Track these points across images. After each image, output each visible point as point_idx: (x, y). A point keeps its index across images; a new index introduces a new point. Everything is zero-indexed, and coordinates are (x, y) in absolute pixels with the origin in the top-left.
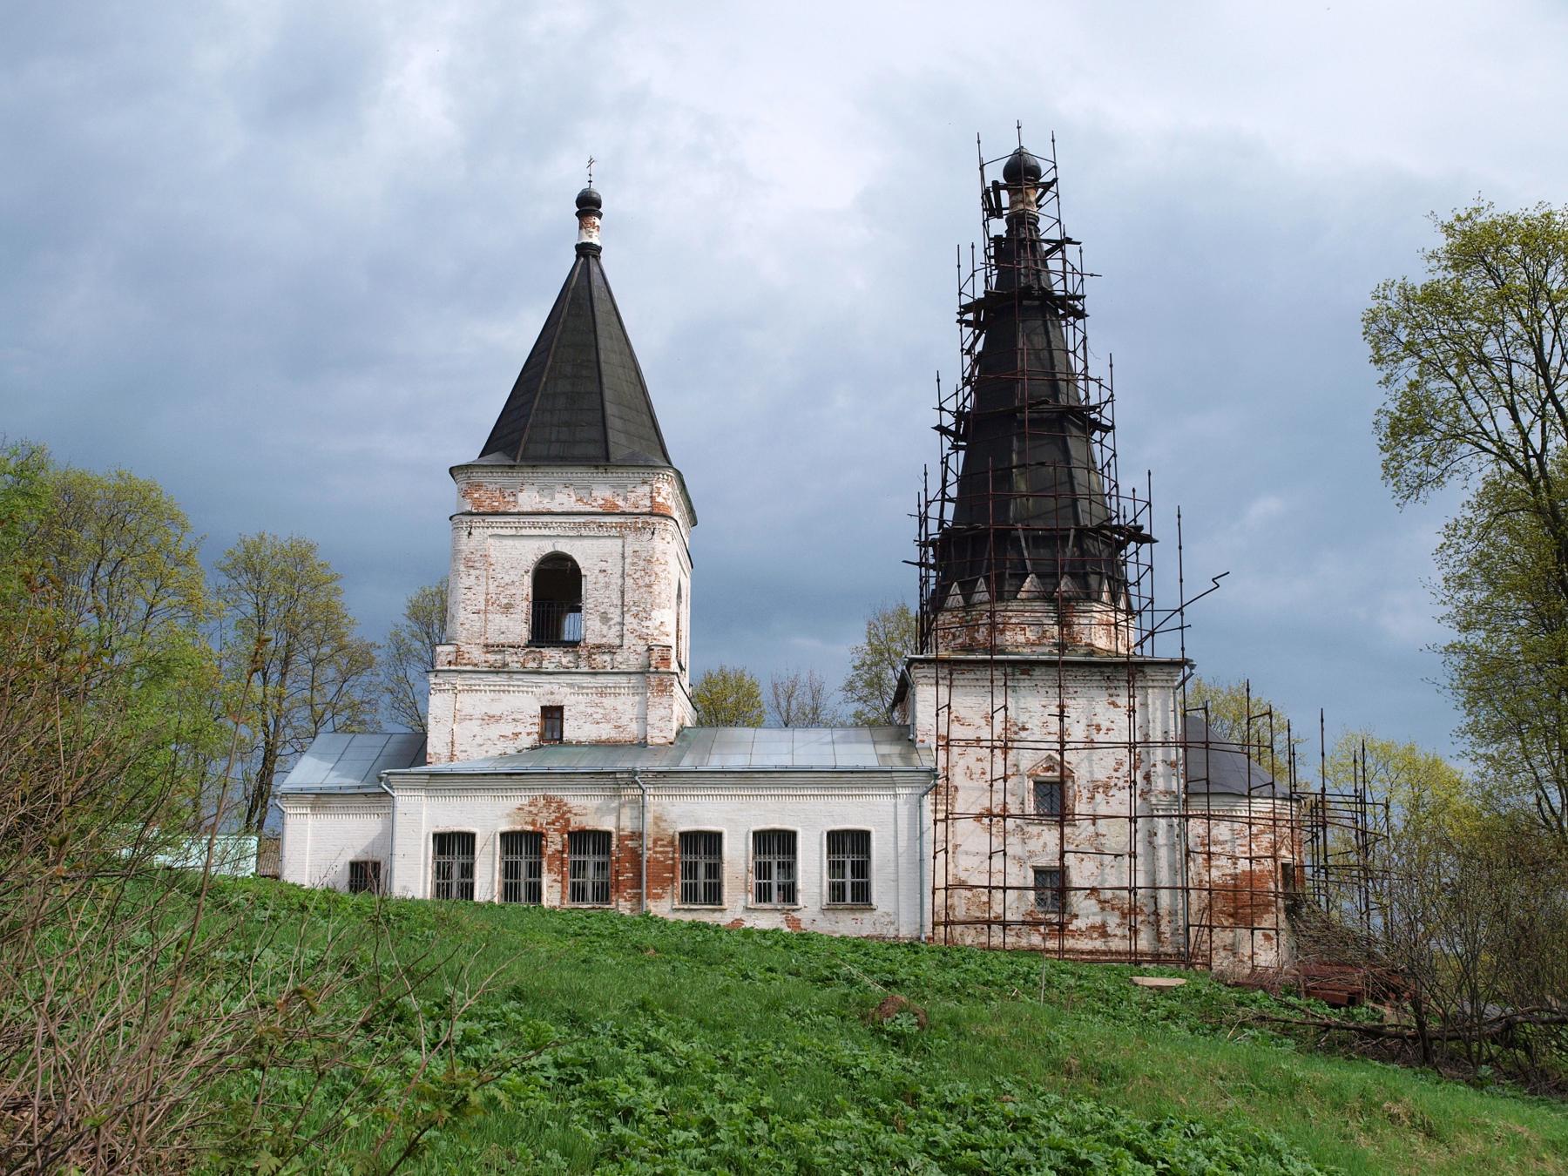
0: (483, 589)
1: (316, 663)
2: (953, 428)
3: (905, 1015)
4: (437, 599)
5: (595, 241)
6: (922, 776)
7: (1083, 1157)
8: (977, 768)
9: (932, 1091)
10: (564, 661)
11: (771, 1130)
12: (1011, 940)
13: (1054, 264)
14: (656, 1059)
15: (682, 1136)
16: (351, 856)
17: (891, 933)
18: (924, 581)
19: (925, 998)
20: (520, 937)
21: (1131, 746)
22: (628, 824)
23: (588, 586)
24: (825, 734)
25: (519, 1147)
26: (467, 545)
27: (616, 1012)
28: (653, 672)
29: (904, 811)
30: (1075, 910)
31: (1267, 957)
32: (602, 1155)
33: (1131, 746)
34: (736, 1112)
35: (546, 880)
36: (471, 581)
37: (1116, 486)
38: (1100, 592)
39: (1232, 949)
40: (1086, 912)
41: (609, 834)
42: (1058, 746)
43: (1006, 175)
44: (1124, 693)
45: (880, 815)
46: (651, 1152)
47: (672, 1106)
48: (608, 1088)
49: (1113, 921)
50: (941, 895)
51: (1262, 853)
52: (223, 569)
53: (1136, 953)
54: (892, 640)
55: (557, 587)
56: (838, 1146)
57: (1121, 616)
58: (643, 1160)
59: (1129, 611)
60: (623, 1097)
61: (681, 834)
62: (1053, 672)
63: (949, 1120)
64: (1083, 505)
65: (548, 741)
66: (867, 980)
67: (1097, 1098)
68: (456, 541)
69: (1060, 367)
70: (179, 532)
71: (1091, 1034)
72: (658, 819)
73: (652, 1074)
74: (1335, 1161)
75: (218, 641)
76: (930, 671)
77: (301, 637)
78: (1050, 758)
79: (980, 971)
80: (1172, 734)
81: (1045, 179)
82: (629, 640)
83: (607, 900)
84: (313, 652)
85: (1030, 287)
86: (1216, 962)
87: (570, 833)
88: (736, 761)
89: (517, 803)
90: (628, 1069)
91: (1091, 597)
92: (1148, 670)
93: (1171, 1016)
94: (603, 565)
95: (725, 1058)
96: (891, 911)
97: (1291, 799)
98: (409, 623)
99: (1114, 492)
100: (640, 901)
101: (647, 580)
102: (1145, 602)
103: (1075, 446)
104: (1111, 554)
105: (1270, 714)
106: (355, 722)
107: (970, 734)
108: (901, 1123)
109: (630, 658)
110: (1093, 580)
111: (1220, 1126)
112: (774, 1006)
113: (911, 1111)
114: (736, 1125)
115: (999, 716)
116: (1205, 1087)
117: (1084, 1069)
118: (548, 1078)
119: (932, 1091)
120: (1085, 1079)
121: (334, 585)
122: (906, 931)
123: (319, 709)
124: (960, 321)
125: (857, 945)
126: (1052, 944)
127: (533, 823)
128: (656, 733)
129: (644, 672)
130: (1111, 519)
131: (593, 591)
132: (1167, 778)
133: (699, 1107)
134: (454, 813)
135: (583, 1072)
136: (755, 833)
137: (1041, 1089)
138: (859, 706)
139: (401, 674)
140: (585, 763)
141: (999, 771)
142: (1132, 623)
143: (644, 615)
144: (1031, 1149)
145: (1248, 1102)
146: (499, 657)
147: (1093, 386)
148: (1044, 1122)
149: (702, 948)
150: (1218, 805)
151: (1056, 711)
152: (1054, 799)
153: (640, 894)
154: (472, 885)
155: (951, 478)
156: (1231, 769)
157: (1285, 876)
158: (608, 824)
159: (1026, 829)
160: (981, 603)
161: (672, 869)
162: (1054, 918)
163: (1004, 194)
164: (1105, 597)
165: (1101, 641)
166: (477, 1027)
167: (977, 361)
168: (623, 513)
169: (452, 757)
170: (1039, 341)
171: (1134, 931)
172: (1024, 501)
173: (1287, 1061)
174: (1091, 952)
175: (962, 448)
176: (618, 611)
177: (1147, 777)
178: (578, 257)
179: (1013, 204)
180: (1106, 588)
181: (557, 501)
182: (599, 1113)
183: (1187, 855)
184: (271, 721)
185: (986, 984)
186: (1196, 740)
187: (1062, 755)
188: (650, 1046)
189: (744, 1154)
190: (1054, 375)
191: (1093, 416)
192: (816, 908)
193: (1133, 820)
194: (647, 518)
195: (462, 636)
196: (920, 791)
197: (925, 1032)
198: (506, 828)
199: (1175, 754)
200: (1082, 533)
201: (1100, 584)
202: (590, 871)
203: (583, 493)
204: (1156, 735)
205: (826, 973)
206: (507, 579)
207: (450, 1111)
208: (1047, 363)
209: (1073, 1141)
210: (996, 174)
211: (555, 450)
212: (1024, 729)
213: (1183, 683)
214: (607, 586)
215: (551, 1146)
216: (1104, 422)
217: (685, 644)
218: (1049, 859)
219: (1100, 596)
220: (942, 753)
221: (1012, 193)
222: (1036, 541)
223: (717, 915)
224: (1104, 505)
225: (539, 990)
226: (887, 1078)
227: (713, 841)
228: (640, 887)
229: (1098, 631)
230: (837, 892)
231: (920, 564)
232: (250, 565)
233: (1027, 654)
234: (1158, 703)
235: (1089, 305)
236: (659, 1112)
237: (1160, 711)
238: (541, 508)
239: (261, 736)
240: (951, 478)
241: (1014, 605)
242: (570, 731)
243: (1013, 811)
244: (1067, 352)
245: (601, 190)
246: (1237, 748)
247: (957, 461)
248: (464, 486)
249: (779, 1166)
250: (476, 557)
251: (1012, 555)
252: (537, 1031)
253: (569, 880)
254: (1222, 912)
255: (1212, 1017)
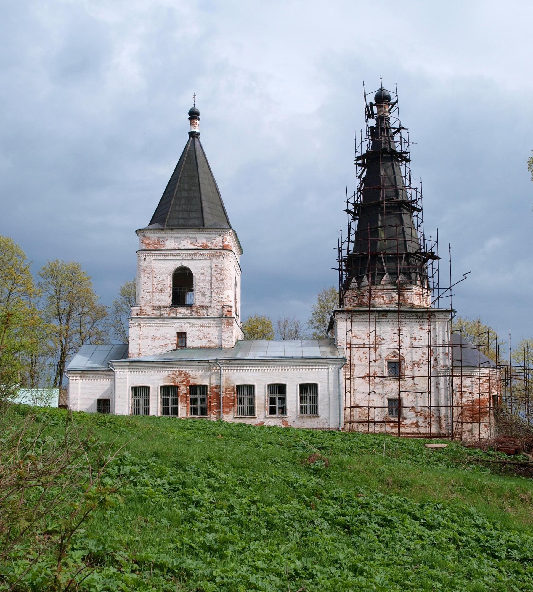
0: (151, 282)
1: (82, 315)
2: (353, 210)
3: (319, 462)
4: (133, 287)
5: (197, 130)
6: (339, 360)
7: (389, 518)
8: (363, 356)
9: (328, 493)
10: (186, 313)
11: (258, 509)
12: (378, 429)
13: (397, 138)
14: (212, 481)
15: (219, 512)
16: (98, 397)
17: (326, 426)
18: (341, 277)
19: (335, 454)
20: (164, 430)
21: (429, 346)
22: (214, 382)
23: (196, 281)
24: (298, 343)
25: (149, 517)
26: (144, 264)
27: (196, 462)
28: (224, 317)
29: (332, 375)
30: (405, 416)
31: (485, 435)
32: (185, 520)
33: (429, 346)
34: (243, 502)
35: (180, 406)
36: (146, 279)
37: (423, 235)
38: (416, 281)
39: (471, 431)
40: (409, 416)
41: (206, 386)
42: (398, 347)
43: (376, 100)
44: (426, 324)
45: (322, 377)
46: (206, 518)
47: (217, 500)
48: (190, 493)
49: (421, 420)
50: (348, 410)
51: (484, 391)
52: (41, 275)
53: (430, 434)
54: (329, 302)
55: (183, 281)
56: (286, 515)
57: (425, 291)
58: (202, 522)
59: (429, 289)
60: (197, 495)
61: (237, 386)
62: (396, 315)
63: (335, 504)
64: (409, 243)
65: (180, 347)
66: (311, 447)
67: (399, 494)
68: (139, 262)
69: (399, 183)
70: (21, 259)
71: (402, 468)
72: (227, 380)
73: (210, 487)
74: (496, 518)
75: (38, 304)
76: (343, 315)
77: (75, 304)
78: (394, 352)
79: (359, 442)
80: (446, 341)
81: (393, 101)
82: (214, 304)
83: (206, 414)
84: (80, 310)
85: (386, 149)
86: (464, 437)
87: (190, 386)
88: (261, 355)
89: (167, 373)
90: (199, 485)
91: (412, 283)
92: (436, 314)
93: (439, 460)
94: (202, 272)
95: (242, 480)
96: (327, 417)
97: (497, 368)
98: (121, 297)
99: (422, 238)
100: (220, 414)
101: (221, 277)
102: (435, 285)
103: (405, 218)
104: (421, 265)
105: (488, 332)
106: (99, 340)
107: (361, 342)
108: (314, 506)
109: (215, 311)
110: (413, 276)
111: (449, 505)
112: (265, 459)
113: (318, 500)
114: (243, 508)
115: (373, 334)
116: (446, 489)
117: (394, 482)
118: (165, 489)
119: (328, 493)
120: (395, 486)
121: (88, 281)
122: (333, 426)
123: (84, 334)
124: (356, 164)
125: (308, 432)
126: (395, 430)
127: (174, 382)
128: (226, 343)
129: (221, 317)
130: (420, 249)
131: (199, 282)
132: (444, 360)
133: (228, 500)
134: (140, 378)
135: (180, 486)
136: (268, 385)
137: (376, 491)
138: (315, 330)
139: (118, 319)
140: (196, 357)
141: (372, 358)
142: (430, 294)
143: (220, 293)
144: (368, 515)
145: (463, 495)
146: (158, 312)
147: (413, 192)
148: (375, 504)
149: (241, 434)
150: (465, 372)
151: (397, 332)
152: (396, 369)
153: (220, 411)
154: (149, 408)
155: (352, 232)
156: (471, 355)
157: (494, 401)
158: (206, 382)
159: (384, 382)
160: (365, 286)
161: (233, 401)
162: (396, 419)
163: (375, 108)
164: (418, 283)
165: (417, 302)
166: (137, 469)
167: (364, 181)
168: (211, 249)
169: (139, 355)
170: (390, 172)
171: (430, 424)
172: (384, 242)
173: (485, 478)
174: (412, 434)
175: (357, 219)
176: (209, 291)
177: (436, 360)
178: (190, 138)
179: (379, 112)
180: (418, 279)
181: (182, 244)
182: (185, 503)
183: (453, 392)
184: (63, 340)
185: (362, 447)
186: (457, 344)
187: (399, 350)
188: (210, 475)
189: (245, 519)
190: (396, 187)
191: (413, 205)
192: (295, 417)
193: (429, 378)
194: (221, 251)
195: (142, 302)
196: (339, 367)
197: (328, 469)
198: (163, 384)
199: (448, 349)
200: (408, 255)
201: (416, 277)
202: (199, 402)
203: (194, 240)
204: (440, 342)
205: (294, 444)
206: (161, 278)
207: (98, 503)
208: (393, 182)
209: (386, 512)
210: (371, 99)
211: (181, 222)
212: (383, 340)
213: (451, 319)
214: (204, 280)
215: (163, 517)
216: (418, 207)
217: (239, 305)
218: (394, 395)
219: (416, 283)
220: (348, 350)
221: (379, 107)
222: (389, 259)
223: (253, 420)
224: (418, 243)
225: (165, 453)
226: (310, 487)
227: (250, 389)
228: (220, 408)
229: (415, 297)
230: (304, 410)
231: (339, 270)
232: (52, 274)
233: (385, 308)
234: (441, 328)
235: (412, 156)
236: (211, 502)
237: (441, 331)
238: (175, 247)
239: (59, 346)
240: (352, 232)
241: (379, 287)
242: (190, 343)
243: (378, 375)
244: (402, 177)
245: (199, 108)
246: (475, 347)
247: (355, 225)
248: (142, 238)
249: (259, 524)
250: (148, 269)
251: (378, 265)
252: (161, 470)
253: (190, 406)
254: (467, 416)
255: (456, 460)
